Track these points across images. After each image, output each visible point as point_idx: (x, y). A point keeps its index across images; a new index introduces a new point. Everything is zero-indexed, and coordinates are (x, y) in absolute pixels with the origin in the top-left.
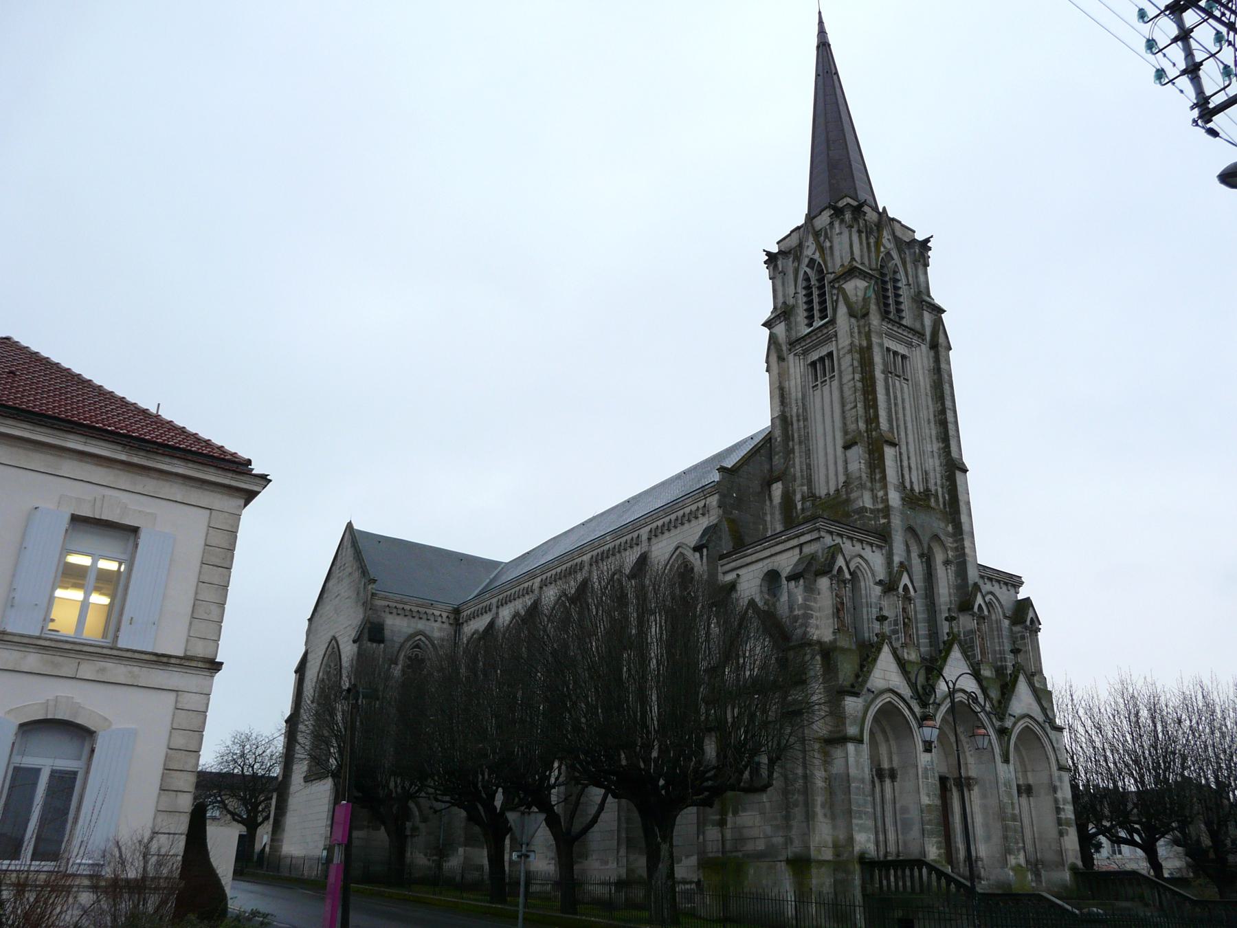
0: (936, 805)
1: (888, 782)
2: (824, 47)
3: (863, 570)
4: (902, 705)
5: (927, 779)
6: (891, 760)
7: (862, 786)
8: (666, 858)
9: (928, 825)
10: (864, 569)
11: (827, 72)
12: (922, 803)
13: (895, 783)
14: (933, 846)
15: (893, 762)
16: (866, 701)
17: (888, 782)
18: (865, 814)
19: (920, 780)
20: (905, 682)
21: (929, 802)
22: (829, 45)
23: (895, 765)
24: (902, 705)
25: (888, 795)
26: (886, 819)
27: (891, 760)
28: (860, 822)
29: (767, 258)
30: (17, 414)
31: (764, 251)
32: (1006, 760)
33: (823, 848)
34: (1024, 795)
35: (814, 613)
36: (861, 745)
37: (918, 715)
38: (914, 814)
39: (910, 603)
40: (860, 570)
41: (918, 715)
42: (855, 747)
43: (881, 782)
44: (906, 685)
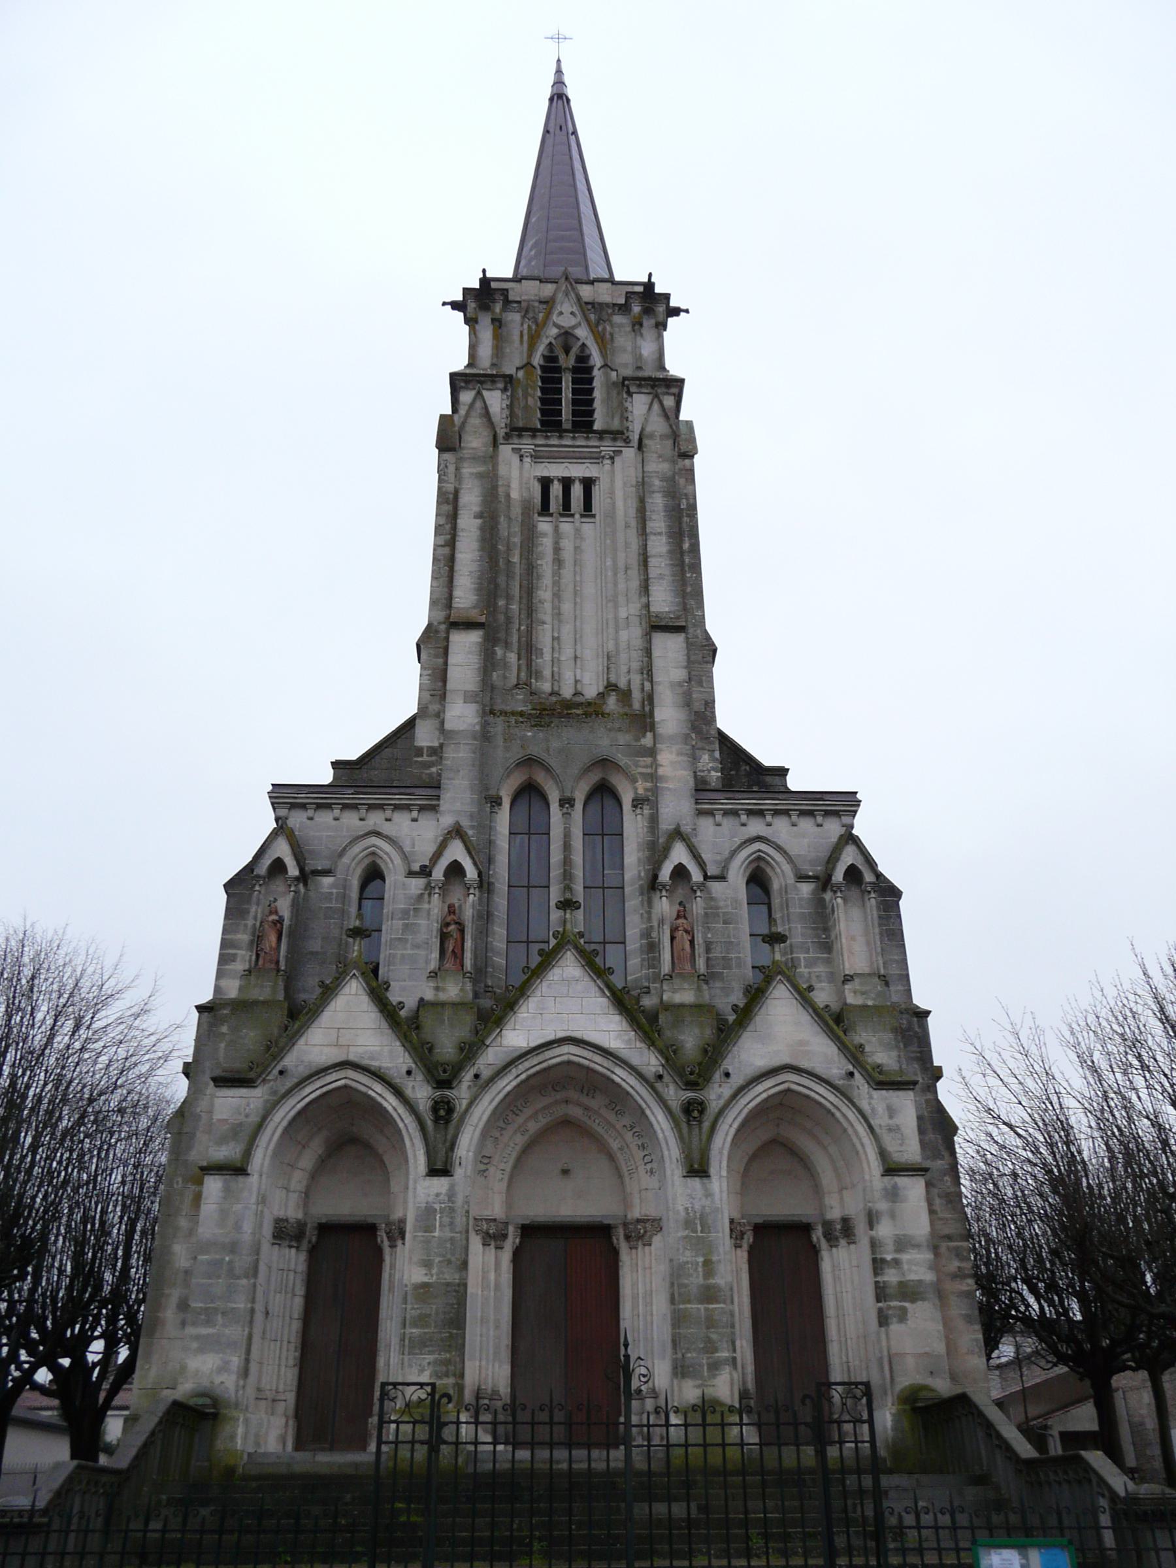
0: (448, 1284)
2: (560, 102)
4: (377, 1091)
5: (429, 1229)
10: (387, 854)
11: (561, 127)
18: (223, 1313)
20: (398, 1043)
21: (426, 1279)
22: (568, 100)
24: (377, 1091)
28: (204, 1331)
29: (477, 286)
30: (48, 1272)
31: (444, 304)
32: (697, 1169)
34: (843, 1242)
36: (241, 1178)
41: (675, 1105)
44: (401, 1049)
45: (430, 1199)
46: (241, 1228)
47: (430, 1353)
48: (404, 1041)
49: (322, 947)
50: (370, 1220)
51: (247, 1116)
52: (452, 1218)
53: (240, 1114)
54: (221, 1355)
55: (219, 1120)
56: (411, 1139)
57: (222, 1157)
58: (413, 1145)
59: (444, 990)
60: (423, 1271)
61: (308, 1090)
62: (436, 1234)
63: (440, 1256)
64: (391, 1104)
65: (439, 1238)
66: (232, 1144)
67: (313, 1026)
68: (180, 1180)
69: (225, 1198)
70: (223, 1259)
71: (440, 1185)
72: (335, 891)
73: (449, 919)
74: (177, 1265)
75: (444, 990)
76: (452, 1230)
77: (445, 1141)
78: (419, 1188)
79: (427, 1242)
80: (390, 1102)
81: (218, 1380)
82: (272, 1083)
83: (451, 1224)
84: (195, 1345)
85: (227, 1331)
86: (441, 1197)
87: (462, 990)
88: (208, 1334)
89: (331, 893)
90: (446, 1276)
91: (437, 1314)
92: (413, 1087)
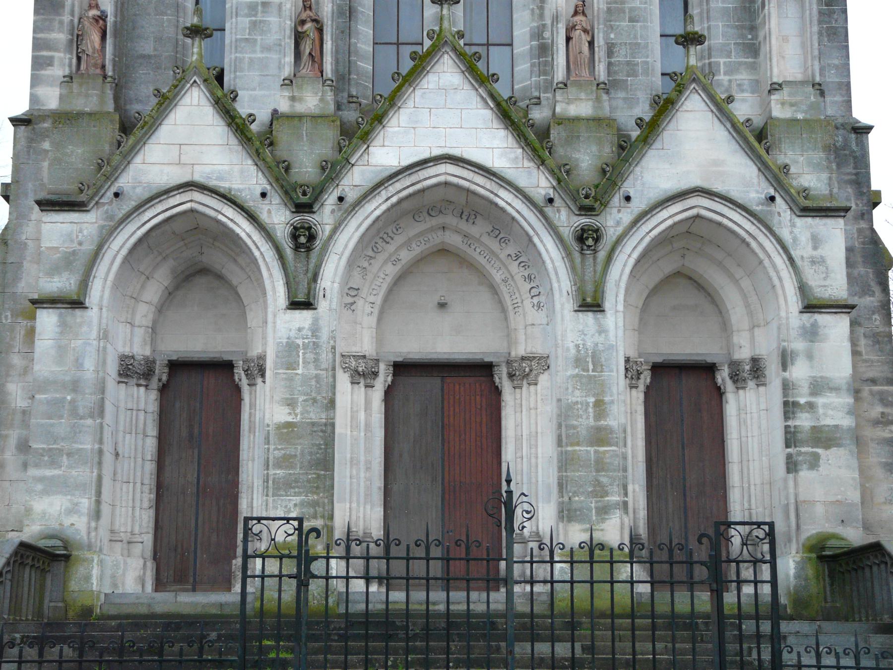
4: (229, 215)
5: (291, 366)
16: (110, 218)
18: (69, 455)
20: (250, 162)
21: (290, 419)
24: (229, 215)
28: (48, 473)
36: (78, 312)
42: (60, 315)
45: (293, 334)
46: (82, 365)
47: (296, 494)
49: (155, 50)
51: (80, 244)
52: (316, 354)
53: (72, 241)
54: (69, 497)
55: (47, 248)
57: (56, 290)
59: (301, 100)
60: (287, 410)
64: (244, 230)
66: (65, 275)
67: (150, 141)
68: (9, 314)
69: (61, 333)
70: (65, 398)
71: (303, 318)
74: (13, 405)
76: (317, 367)
77: (307, 271)
78: (278, 322)
79: (290, 379)
80: (243, 228)
81: (67, 522)
82: (106, 207)
83: (316, 360)
85: (74, 473)
86: (304, 332)
87: (322, 100)
88: (53, 476)
90: (312, 415)
92: (269, 211)
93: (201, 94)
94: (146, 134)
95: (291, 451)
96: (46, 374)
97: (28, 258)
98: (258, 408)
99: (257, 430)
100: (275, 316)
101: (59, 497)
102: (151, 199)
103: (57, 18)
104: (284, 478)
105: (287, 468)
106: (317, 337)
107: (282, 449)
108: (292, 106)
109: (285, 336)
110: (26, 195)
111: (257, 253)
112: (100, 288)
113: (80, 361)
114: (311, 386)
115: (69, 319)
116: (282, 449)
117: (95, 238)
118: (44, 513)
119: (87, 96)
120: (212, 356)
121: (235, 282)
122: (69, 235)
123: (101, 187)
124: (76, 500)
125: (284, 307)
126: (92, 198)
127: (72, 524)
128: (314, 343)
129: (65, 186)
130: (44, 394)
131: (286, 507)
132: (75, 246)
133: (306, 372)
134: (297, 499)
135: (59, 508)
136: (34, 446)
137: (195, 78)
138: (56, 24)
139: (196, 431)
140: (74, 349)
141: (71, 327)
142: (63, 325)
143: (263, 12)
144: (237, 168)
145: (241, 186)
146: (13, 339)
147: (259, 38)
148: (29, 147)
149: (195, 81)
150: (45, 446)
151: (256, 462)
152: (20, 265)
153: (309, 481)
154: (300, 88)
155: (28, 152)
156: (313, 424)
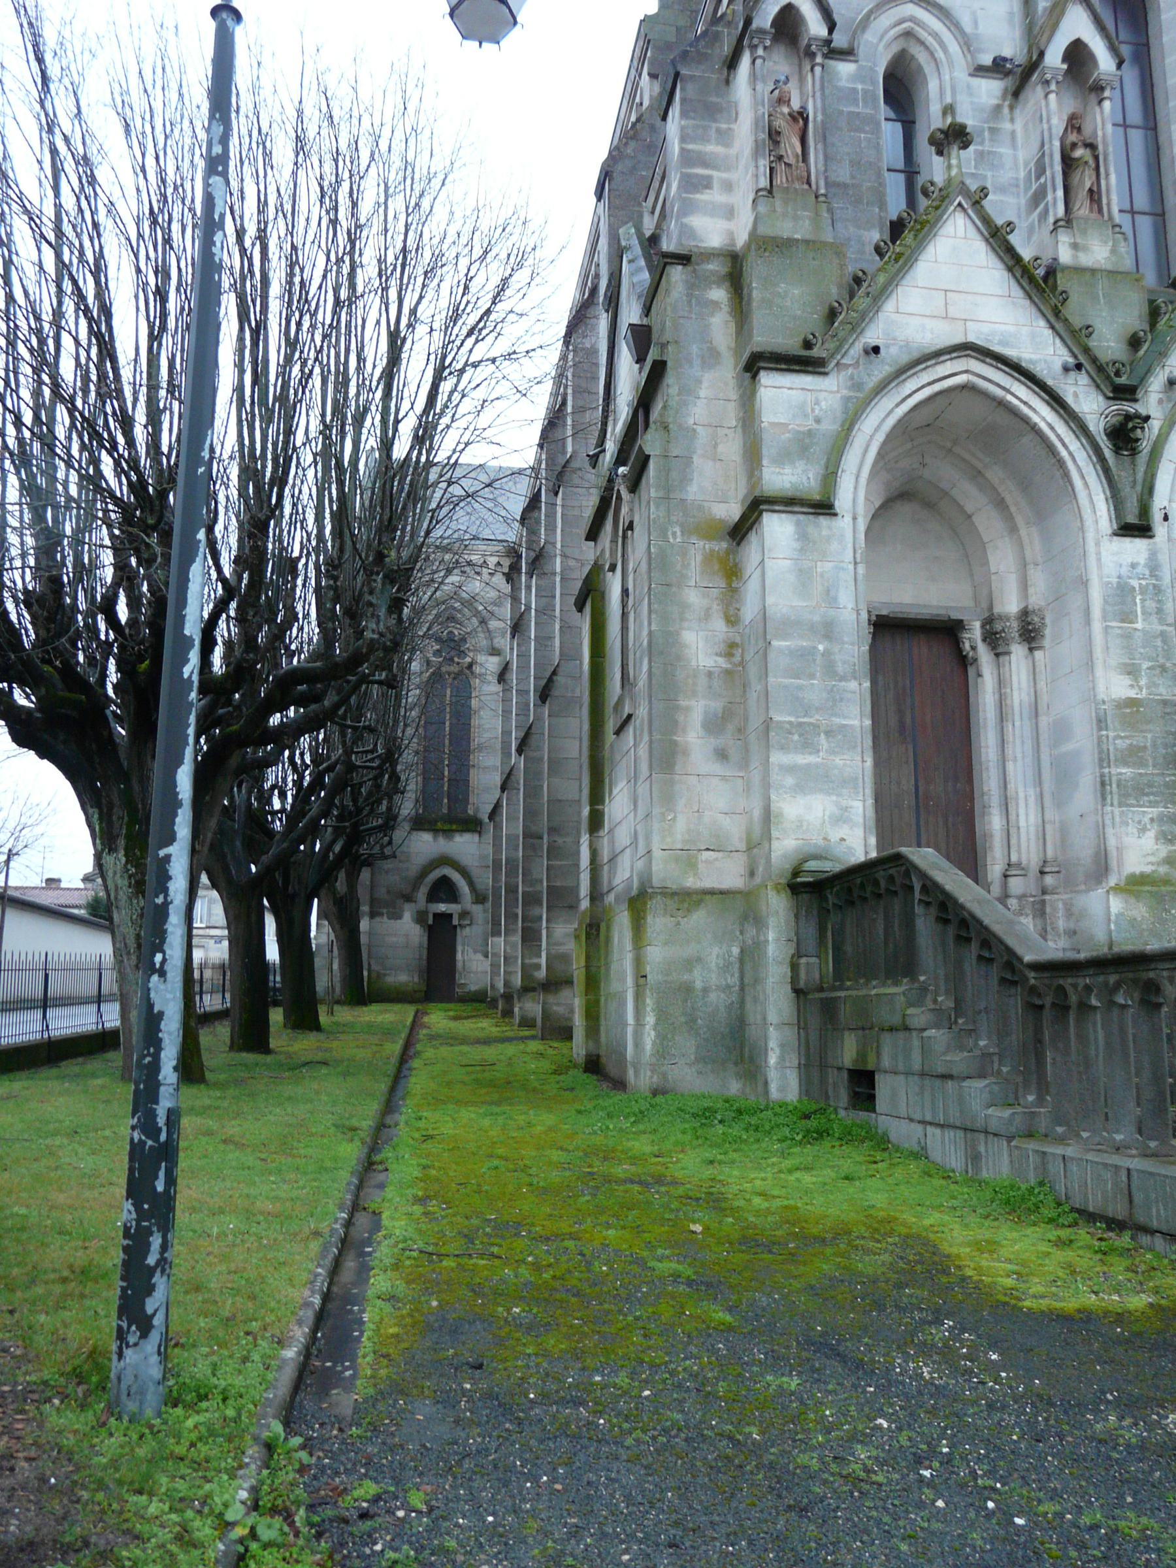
1: (1018, 651)
3: (930, 40)
4: (1020, 394)
5: (1127, 617)
6: (1024, 585)
7: (821, 647)
8: (123, 897)
9: (1126, 764)
10: (936, 36)
12: (1101, 695)
13: (1038, 654)
14: (1143, 830)
15: (1031, 591)
16: (857, 386)
17: (1018, 651)
18: (828, 733)
19: (1097, 626)
20: (1042, 323)
21: (1132, 694)
23: (1036, 599)
24: (1020, 394)
25: (1019, 694)
26: (1010, 766)
27: (1024, 585)
28: (802, 759)
33: (706, 855)
35: (714, 173)
36: (823, 521)
37: (1097, 426)
38: (1082, 740)
39: (1100, 102)
40: (922, 43)
41: (1097, 426)
42: (798, 524)
43: (997, 655)
44: (1048, 332)
45: (1124, 571)
46: (835, 599)
47: (1152, 804)
48: (1053, 320)
49: (853, 177)
50: (955, 615)
51: (818, 421)
52: (1159, 601)
53: (806, 416)
54: (834, 798)
55: (773, 424)
56: (1083, 477)
57: (788, 485)
58: (1086, 485)
59: (1085, 249)
60: (1127, 681)
61: (910, 386)
62: (1139, 625)
63: (1150, 659)
64: (1044, 419)
65: (1143, 630)
66: (800, 465)
67: (904, 282)
68: (677, 530)
69: (802, 550)
70: (815, 648)
71: (1136, 548)
72: (860, 87)
73: (1073, 137)
74: (694, 663)
75: (1085, 249)
76: (1162, 621)
77: (1134, 482)
78: (1104, 554)
79: (1127, 636)
80: (1042, 414)
81: (834, 836)
82: (850, 370)
83: (1159, 611)
84: (790, 781)
85: (838, 761)
86: (1140, 569)
87: (1114, 251)
88: (809, 765)
89: (855, 90)
90: (1162, 690)
91: (1154, 745)
92: (1076, 395)
93: (968, 222)
94: (899, 271)
95: (1138, 740)
96: (784, 610)
97: (699, 452)
98: (1015, 686)
99: (1017, 717)
100: (1098, 544)
101: (820, 796)
102: (918, 362)
103: (714, 125)
104: (1133, 779)
105: (1134, 765)
106: (1157, 578)
107: (1126, 737)
108: (1075, 257)
109: (1115, 574)
110: (690, 362)
111: (1064, 453)
112: (851, 487)
113: (832, 593)
114: (1156, 647)
115: (811, 529)
116: (1126, 737)
117: (839, 414)
118: (801, 821)
119: (796, 218)
120: (935, 612)
121: (969, 508)
122: (802, 406)
123: (845, 340)
124: (844, 803)
125: (1110, 531)
126: (832, 356)
127: (843, 840)
128: (1155, 586)
129: (780, 340)
130: (784, 639)
131: (1139, 822)
132: (810, 423)
133: (1148, 627)
134: (1154, 812)
135: (820, 814)
136: (777, 718)
137: (960, 198)
138: (713, 133)
139: (908, 720)
140: (822, 576)
141: (815, 543)
142: (803, 536)
143: (991, 140)
144: (1025, 330)
145: (1033, 357)
146: (686, 566)
147: (989, 174)
148: (690, 296)
149: (960, 205)
150: (793, 719)
151: (1020, 763)
152: (688, 460)
153: (1167, 785)
154: (1084, 232)
155: (690, 302)
156: (1165, 703)
